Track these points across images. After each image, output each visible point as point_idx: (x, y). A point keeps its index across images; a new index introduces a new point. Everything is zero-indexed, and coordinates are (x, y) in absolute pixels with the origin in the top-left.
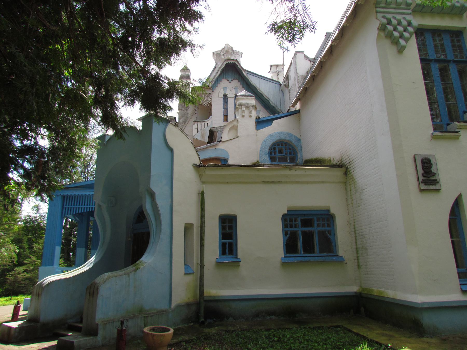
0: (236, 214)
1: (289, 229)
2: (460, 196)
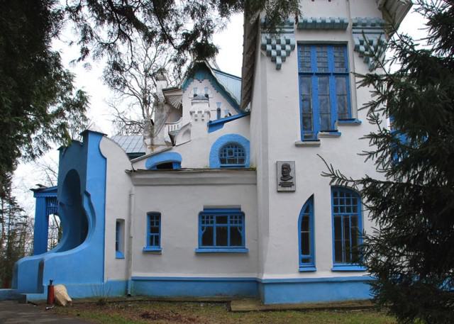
0: (160, 211)
1: (205, 225)
2: (312, 198)
